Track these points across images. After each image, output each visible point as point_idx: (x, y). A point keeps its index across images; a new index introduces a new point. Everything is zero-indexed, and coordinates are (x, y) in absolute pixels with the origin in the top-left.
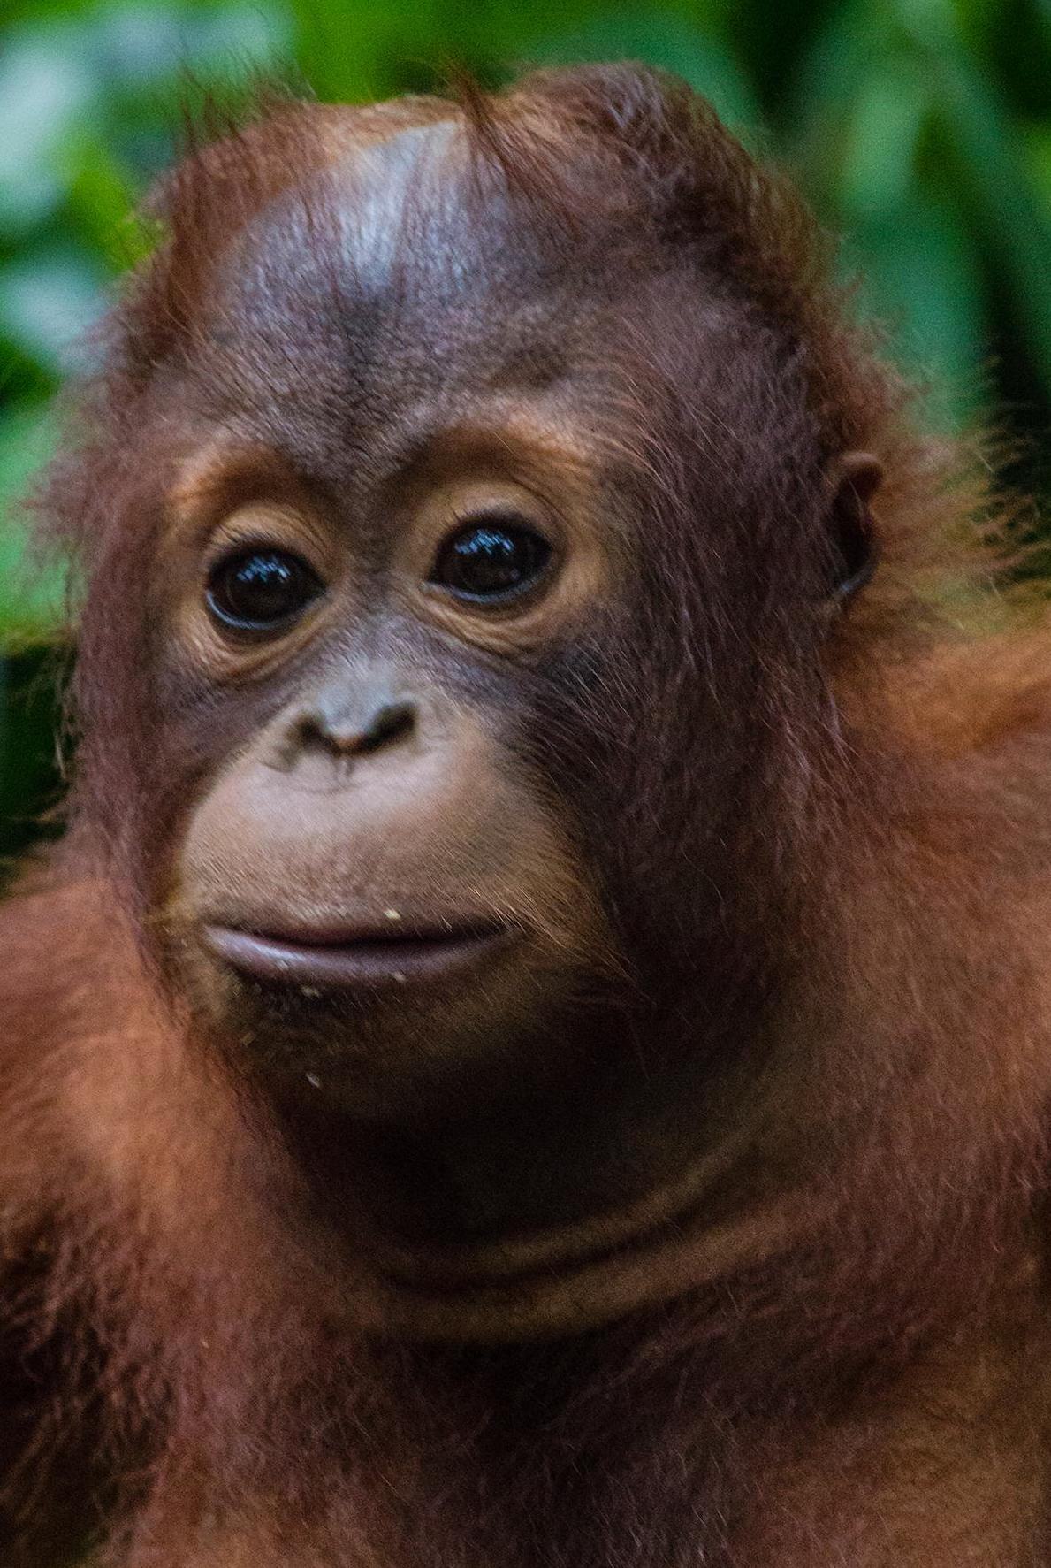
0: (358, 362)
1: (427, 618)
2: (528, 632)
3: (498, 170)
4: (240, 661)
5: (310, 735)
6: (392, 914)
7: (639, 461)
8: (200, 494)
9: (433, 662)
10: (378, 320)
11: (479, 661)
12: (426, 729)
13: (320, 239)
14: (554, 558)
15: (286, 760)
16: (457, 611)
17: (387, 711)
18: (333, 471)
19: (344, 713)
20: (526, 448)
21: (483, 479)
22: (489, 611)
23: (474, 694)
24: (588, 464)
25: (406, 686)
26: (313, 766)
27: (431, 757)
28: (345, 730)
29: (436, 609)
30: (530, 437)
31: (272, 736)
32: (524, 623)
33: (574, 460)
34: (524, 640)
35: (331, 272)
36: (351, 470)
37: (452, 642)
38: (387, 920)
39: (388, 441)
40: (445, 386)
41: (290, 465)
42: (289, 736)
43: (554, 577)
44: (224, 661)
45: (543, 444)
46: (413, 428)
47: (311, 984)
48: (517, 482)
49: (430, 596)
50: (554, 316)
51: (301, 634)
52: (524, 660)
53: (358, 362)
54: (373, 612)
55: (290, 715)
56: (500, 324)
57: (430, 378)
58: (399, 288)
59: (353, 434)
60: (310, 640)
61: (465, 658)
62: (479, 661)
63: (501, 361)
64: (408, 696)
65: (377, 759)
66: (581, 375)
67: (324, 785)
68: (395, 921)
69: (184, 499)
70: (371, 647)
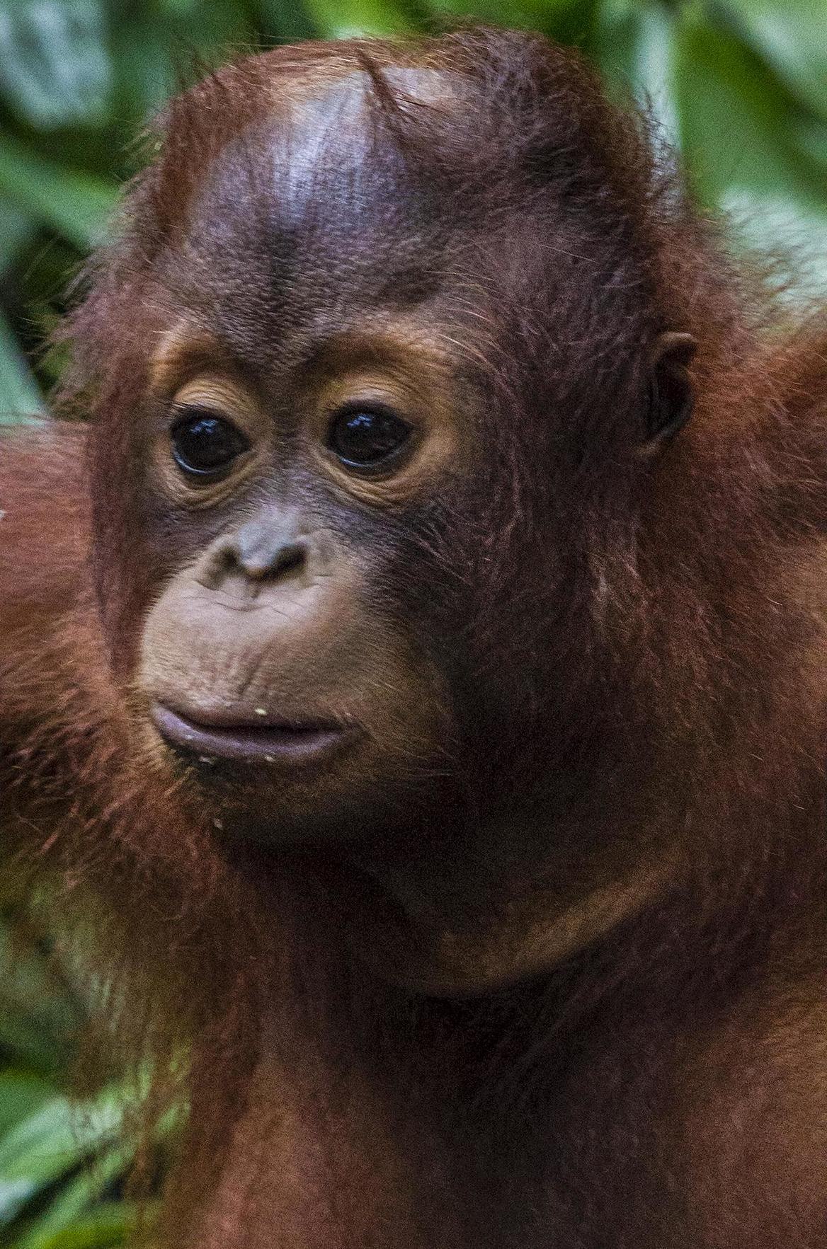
0: (279, 275)
1: (322, 474)
2: (393, 490)
3: (403, 106)
4: (192, 494)
5: (229, 562)
6: (261, 711)
7: (487, 365)
8: (167, 363)
9: (324, 508)
10: (296, 245)
11: (362, 512)
12: (312, 566)
13: (258, 178)
14: (414, 436)
15: (213, 580)
16: (346, 473)
17: (285, 550)
18: (258, 358)
19: (257, 548)
20: (404, 350)
21: (364, 371)
22: (365, 474)
23: (354, 537)
24: (446, 363)
25: (305, 531)
26: (234, 587)
27: (312, 591)
28: (255, 562)
29: (328, 466)
30: (403, 342)
31: (204, 560)
32: (393, 483)
33: (435, 360)
34: (393, 496)
35: (262, 204)
36: (271, 358)
37: (340, 493)
38: (257, 715)
39: (299, 340)
40: (341, 298)
41: (228, 351)
42: (216, 561)
43: (415, 448)
44: (182, 492)
45: (412, 347)
46: (319, 332)
47: (207, 755)
48: (390, 374)
49: (328, 458)
50: (430, 245)
51: (235, 478)
52: (392, 511)
53: (279, 275)
54: (286, 467)
55: (218, 544)
56: (385, 251)
57: (328, 293)
58: (314, 216)
59: (273, 332)
60: (241, 484)
61: (352, 509)
62: (362, 512)
63: (385, 281)
64: (302, 538)
65: (276, 588)
66: (448, 289)
67: (240, 604)
68: (262, 716)
69: (159, 362)
70: (284, 496)
